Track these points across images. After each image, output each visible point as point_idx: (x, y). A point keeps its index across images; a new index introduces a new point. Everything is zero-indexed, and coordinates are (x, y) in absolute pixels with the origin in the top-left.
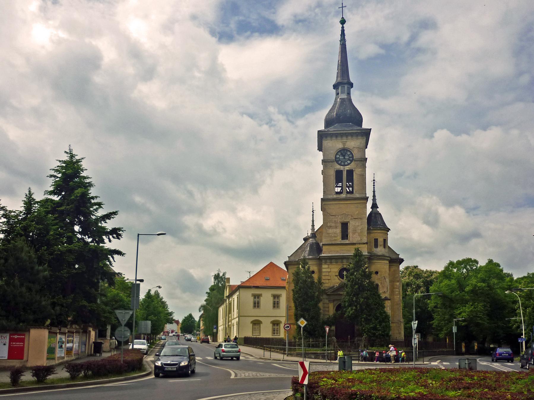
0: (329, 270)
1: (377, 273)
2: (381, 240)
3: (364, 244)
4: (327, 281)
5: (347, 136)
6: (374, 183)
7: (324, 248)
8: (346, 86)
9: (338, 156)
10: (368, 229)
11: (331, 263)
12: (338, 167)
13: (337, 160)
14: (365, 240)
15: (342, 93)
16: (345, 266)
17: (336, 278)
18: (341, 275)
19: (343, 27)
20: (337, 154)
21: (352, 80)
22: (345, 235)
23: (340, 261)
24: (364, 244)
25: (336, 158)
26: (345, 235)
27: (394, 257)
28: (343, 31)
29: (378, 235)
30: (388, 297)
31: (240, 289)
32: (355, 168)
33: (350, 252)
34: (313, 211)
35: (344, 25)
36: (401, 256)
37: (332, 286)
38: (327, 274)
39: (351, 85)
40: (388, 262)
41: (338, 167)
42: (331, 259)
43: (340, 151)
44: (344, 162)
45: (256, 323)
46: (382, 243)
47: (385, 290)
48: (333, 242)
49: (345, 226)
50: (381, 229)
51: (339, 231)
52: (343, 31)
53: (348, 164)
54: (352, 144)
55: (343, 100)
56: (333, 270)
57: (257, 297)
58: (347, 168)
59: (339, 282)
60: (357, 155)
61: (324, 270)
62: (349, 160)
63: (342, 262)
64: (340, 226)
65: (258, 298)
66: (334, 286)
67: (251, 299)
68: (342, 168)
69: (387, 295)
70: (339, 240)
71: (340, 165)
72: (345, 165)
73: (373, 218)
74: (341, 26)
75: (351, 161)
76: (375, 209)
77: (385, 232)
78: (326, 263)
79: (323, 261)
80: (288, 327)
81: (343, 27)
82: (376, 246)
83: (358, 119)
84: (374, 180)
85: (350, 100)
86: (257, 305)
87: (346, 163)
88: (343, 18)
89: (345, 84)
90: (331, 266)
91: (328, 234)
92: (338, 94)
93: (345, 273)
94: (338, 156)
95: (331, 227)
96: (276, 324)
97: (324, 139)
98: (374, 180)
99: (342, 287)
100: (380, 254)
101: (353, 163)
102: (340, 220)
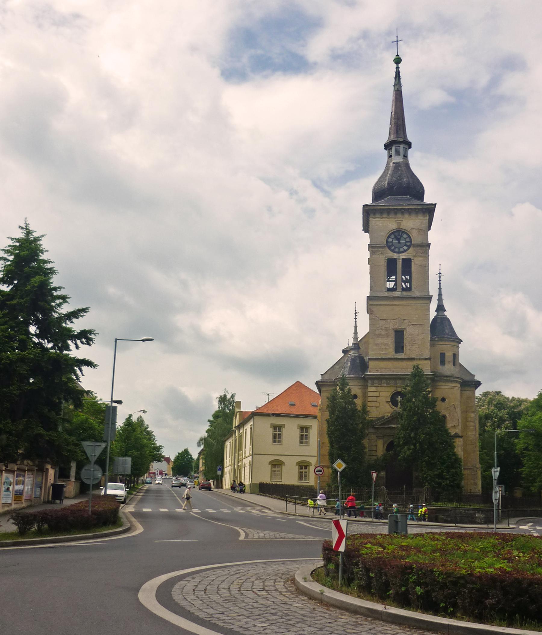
0: (377, 394)
1: (443, 400)
2: (449, 355)
3: (426, 359)
4: (375, 410)
5: (403, 213)
6: (440, 277)
7: (371, 364)
8: (402, 146)
9: (390, 240)
10: (432, 339)
11: (380, 384)
12: (391, 254)
13: (389, 246)
14: (427, 354)
15: (397, 154)
16: (399, 390)
17: (387, 405)
18: (393, 401)
19: (397, 68)
20: (389, 237)
21: (410, 138)
22: (399, 347)
23: (392, 382)
24: (426, 359)
25: (387, 242)
26: (399, 347)
27: (467, 378)
28: (398, 73)
29: (447, 348)
30: (460, 434)
31: (255, 417)
32: (413, 256)
33: (406, 369)
34: (356, 314)
35: (400, 65)
36: (477, 378)
37: (381, 416)
38: (375, 399)
39: (409, 145)
40: (459, 385)
41: (391, 254)
42: (380, 379)
43: (393, 233)
44: (399, 248)
45: (277, 464)
46: (451, 359)
47: (455, 423)
48: (384, 356)
49: (399, 335)
50: (449, 340)
51: (391, 341)
52: (398, 73)
53: (405, 251)
54: (410, 223)
55: (397, 165)
56: (382, 394)
57: (278, 428)
58: (403, 256)
59: (392, 410)
60: (416, 238)
61: (370, 394)
62: (406, 245)
63: (396, 384)
64: (392, 334)
65: (280, 429)
66: (384, 417)
67: (270, 432)
68: (395, 256)
69: (458, 431)
70: (391, 353)
71: (393, 251)
72: (399, 252)
73: (438, 325)
74: (395, 66)
75: (409, 247)
76: (440, 313)
77: (455, 344)
78: (373, 384)
79: (370, 382)
80: (320, 471)
81: (397, 68)
82: (443, 362)
83: (416, 190)
84: (440, 273)
85: (407, 165)
86: (277, 439)
87: (402, 250)
88: (397, 55)
89: (400, 143)
90: (380, 389)
91: (376, 344)
92: (390, 156)
93: (399, 399)
94: (390, 240)
95: (380, 335)
96: (303, 466)
97: (372, 216)
98: (440, 273)
99: (394, 418)
100: (448, 373)
101: (411, 249)
102: (392, 326)
